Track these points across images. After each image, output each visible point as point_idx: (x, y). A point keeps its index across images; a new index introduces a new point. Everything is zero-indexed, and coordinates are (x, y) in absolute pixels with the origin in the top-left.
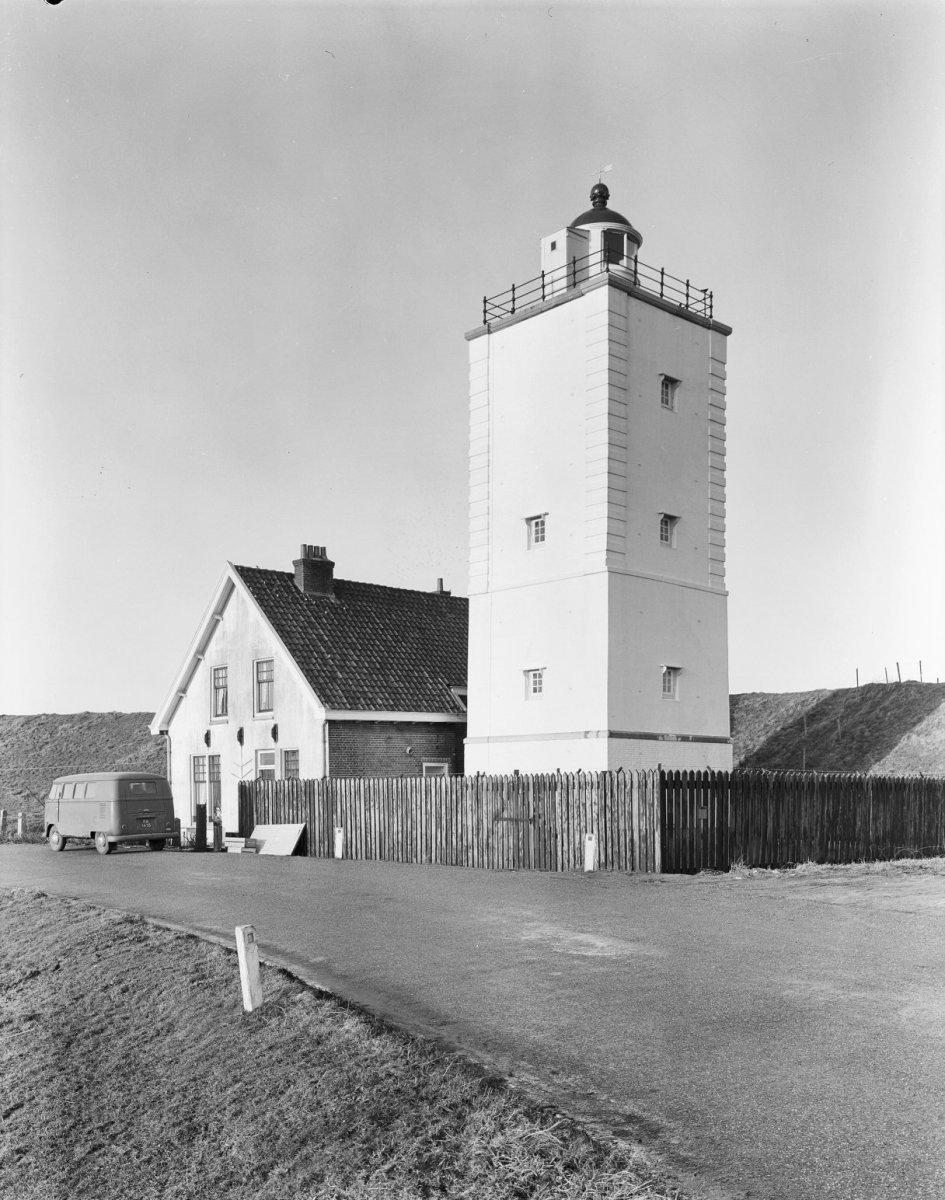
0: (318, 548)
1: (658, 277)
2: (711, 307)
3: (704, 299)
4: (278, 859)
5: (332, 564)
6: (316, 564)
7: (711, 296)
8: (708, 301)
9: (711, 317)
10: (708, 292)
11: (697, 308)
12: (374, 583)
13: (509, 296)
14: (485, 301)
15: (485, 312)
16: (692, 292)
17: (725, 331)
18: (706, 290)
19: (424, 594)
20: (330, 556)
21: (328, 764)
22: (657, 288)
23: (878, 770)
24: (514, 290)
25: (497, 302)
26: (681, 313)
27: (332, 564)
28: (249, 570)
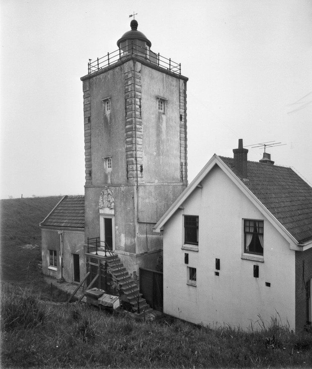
9: (180, 73)
11: (174, 70)
13: (96, 63)
16: (172, 63)
17: (186, 80)
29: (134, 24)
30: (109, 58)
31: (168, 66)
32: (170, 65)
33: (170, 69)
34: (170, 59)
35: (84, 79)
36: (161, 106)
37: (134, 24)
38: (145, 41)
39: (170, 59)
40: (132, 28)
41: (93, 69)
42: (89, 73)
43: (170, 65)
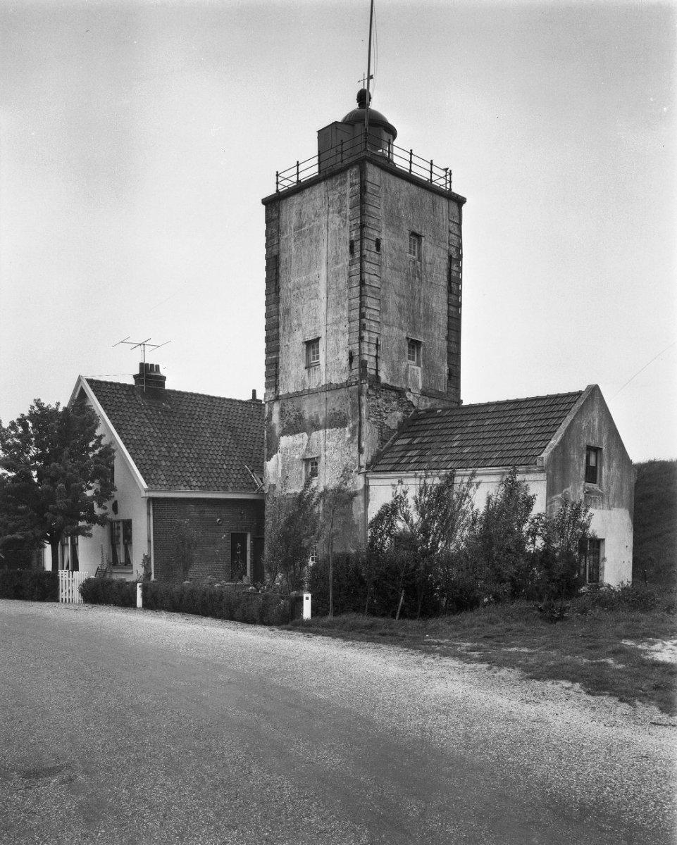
0: (153, 365)
1: (428, 167)
2: (450, 182)
3: (446, 176)
4: (237, 613)
5: (164, 378)
6: (149, 377)
7: (450, 174)
8: (448, 178)
9: (450, 189)
10: (448, 171)
11: (440, 183)
12: (200, 393)
13: (295, 170)
14: (277, 175)
15: (277, 183)
16: (435, 169)
17: (460, 201)
18: (446, 169)
19: (240, 401)
20: (163, 372)
21: (152, 533)
22: (428, 175)
23: (369, 522)
24: (298, 165)
25: (285, 175)
26: (427, 186)
27: (164, 378)
28: (98, 382)
29: (363, 97)
30: (296, 167)
31: (428, 175)
32: (431, 172)
33: (431, 180)
34: (411, 150)
35: (267, 202)
36: (413, 352)
37: (363, 97)
38: (381, 126)
39: (411, 150)
40: (359, 105)
41: (286, 183)
42: (277, 191)
43: (431, 172)
